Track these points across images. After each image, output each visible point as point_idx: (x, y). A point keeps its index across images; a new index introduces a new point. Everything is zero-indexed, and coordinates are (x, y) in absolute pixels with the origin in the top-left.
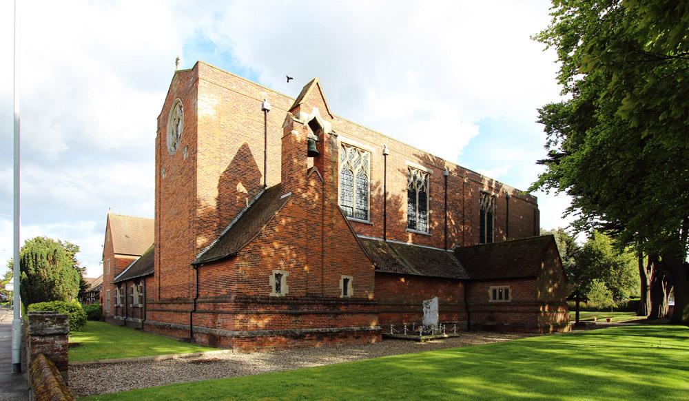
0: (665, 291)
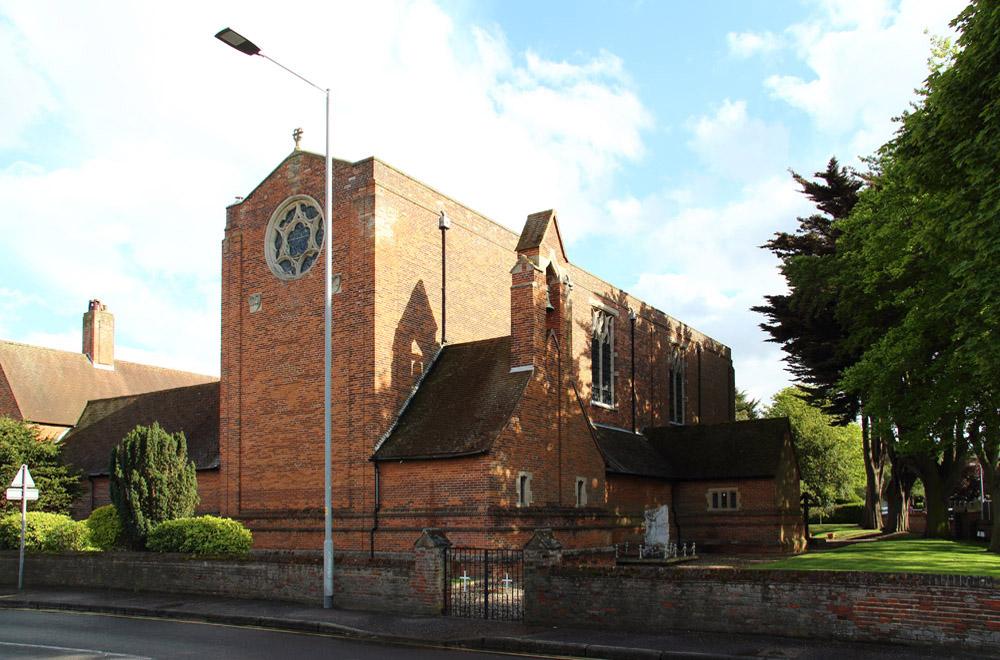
0: (903, 494)
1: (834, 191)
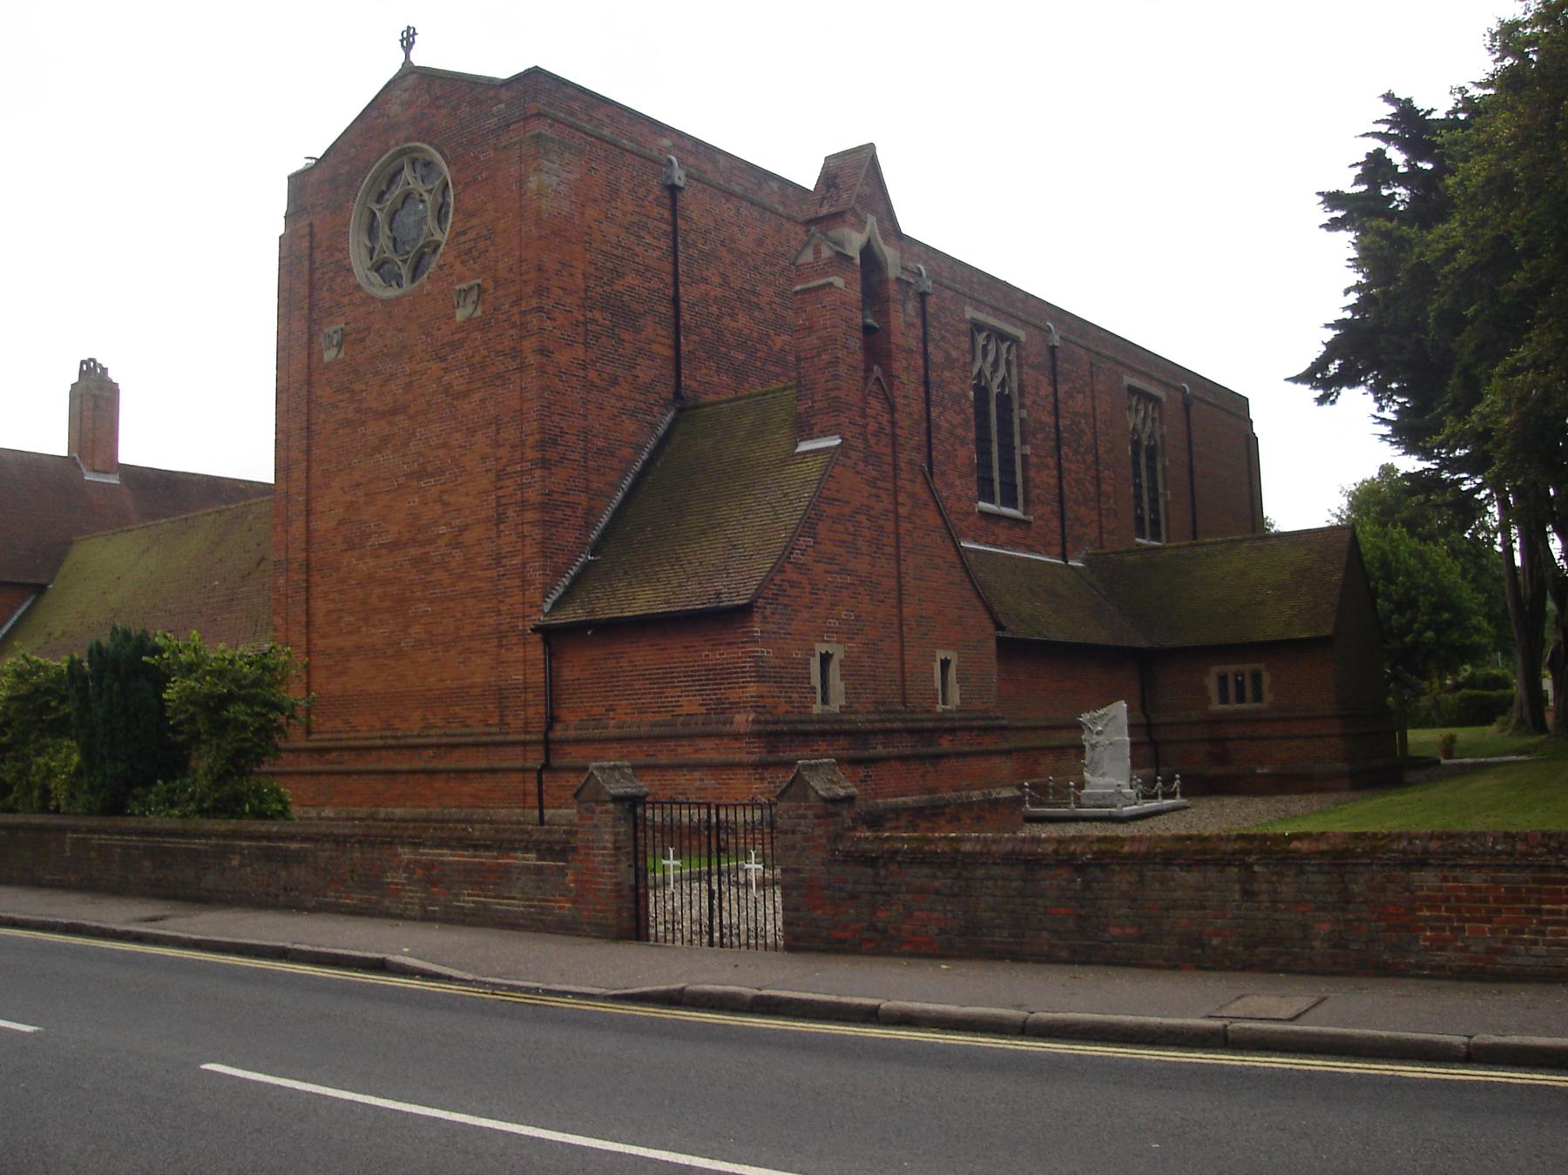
1: (1408, 123)
